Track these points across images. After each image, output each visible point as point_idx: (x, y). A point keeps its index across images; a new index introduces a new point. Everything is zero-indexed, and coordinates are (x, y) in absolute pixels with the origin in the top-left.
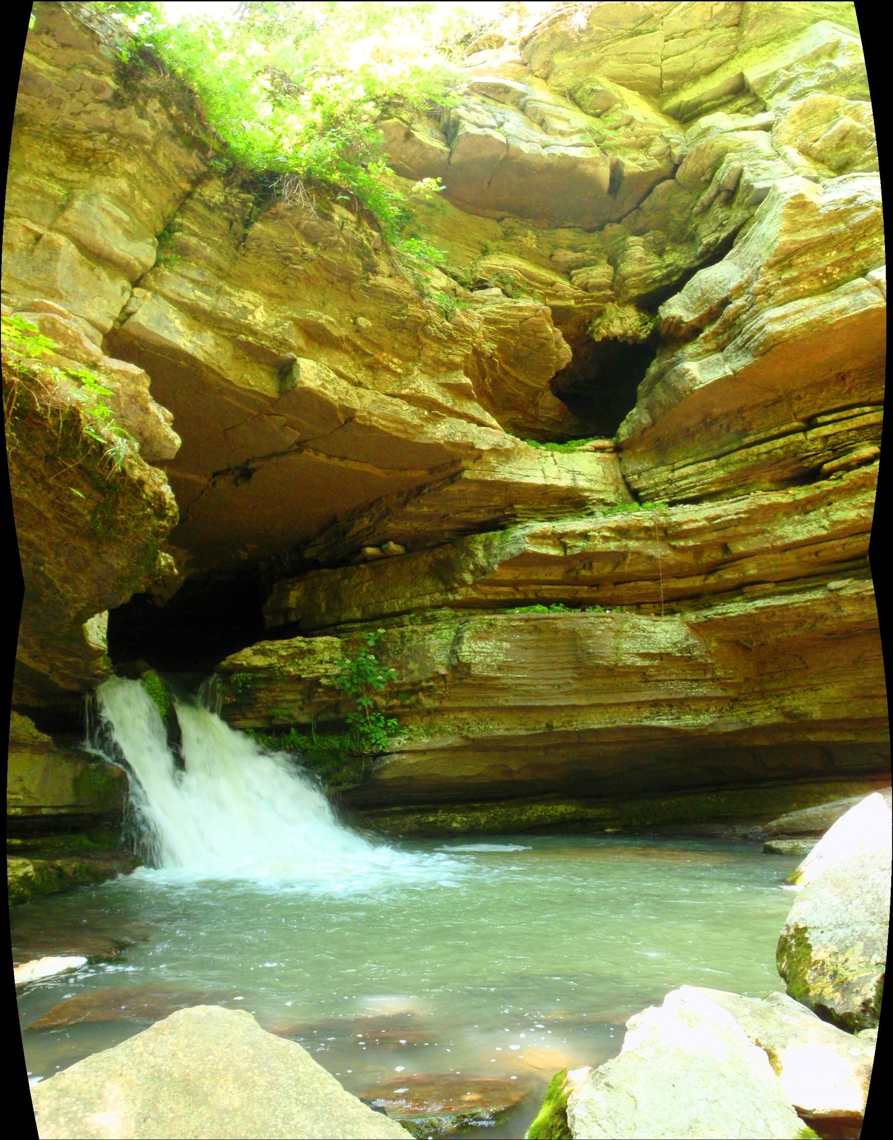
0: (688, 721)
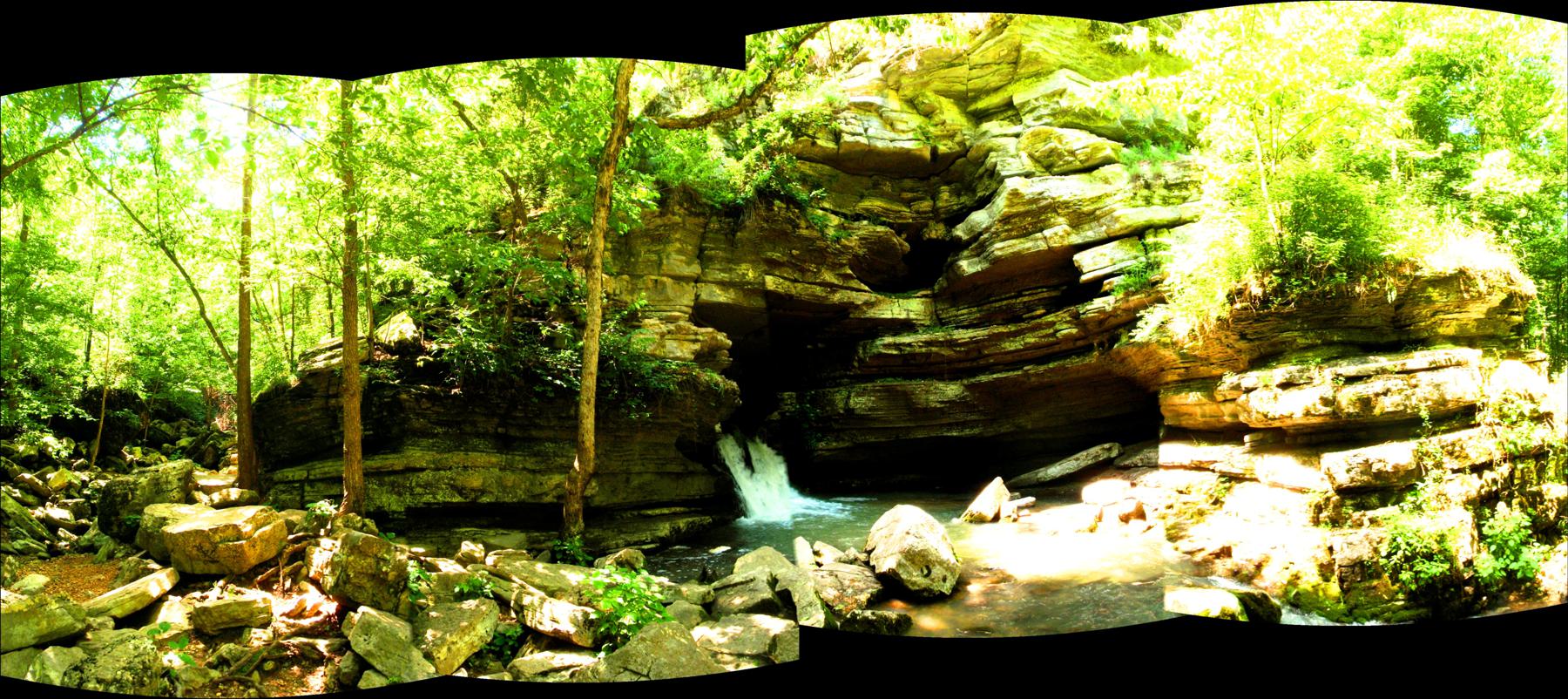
0: (967, 432)
